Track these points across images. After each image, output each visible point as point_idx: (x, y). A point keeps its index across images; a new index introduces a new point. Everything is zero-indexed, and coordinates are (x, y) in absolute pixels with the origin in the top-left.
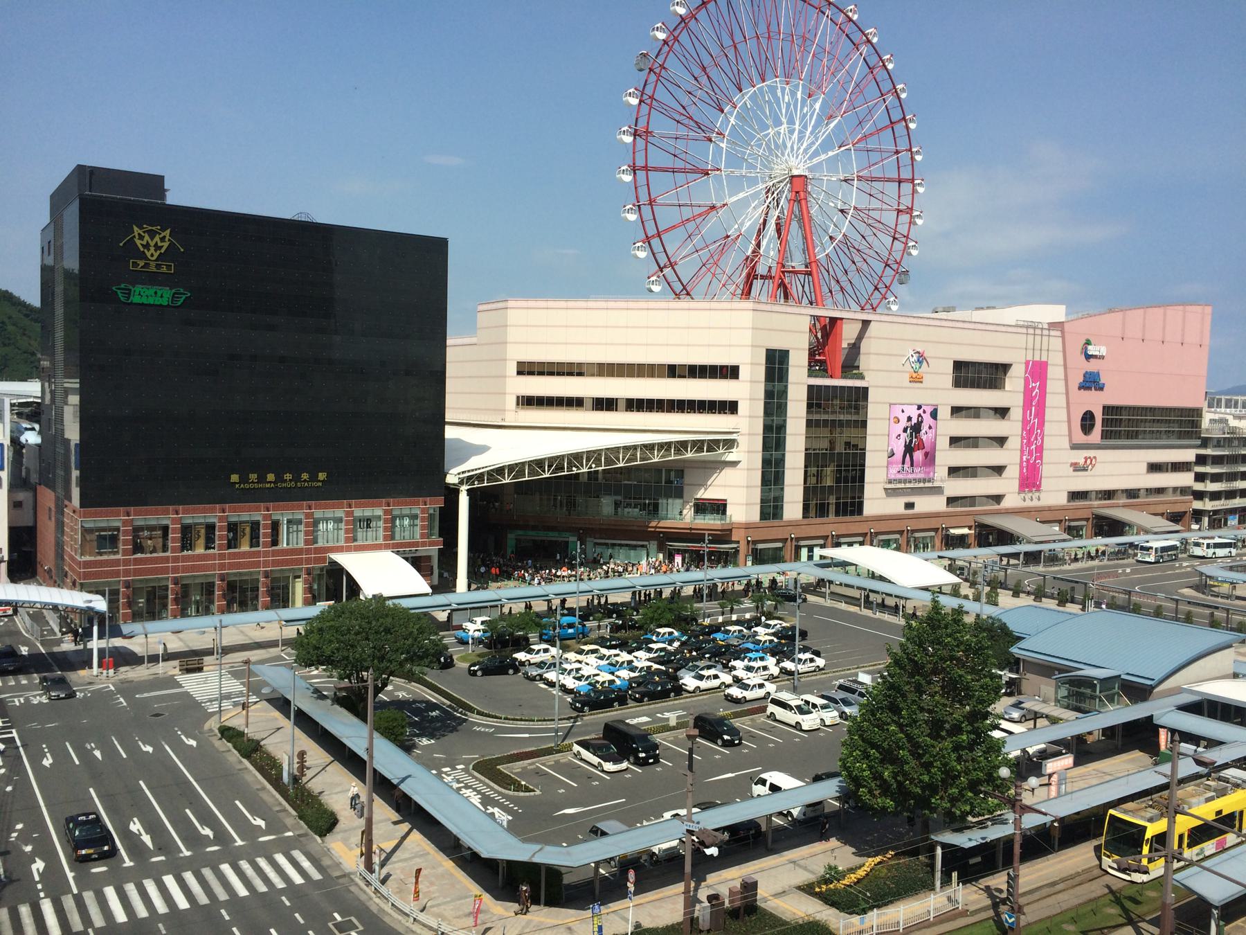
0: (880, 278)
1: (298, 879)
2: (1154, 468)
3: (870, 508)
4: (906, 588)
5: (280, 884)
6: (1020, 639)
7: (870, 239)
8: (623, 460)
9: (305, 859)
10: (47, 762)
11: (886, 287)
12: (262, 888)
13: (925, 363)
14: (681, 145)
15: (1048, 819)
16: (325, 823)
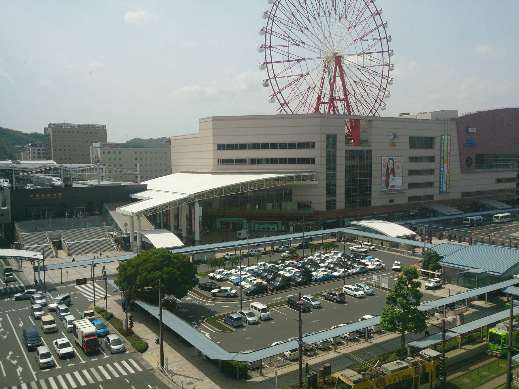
0: (378, 97)
1: (132, 371)
2: (499, 181)
3: (374, 203)
4: (391, 237)
5: (125, 374)
6: (442, 257)
7: (372, 80)
8: (265, 185)
9: (135, 362)
10: (21, 325)
11: (381, 100)
12: (117, 376)
13: (396, 138)
14: (286, 49)
15: (457, 334)
16: (143, 348)
